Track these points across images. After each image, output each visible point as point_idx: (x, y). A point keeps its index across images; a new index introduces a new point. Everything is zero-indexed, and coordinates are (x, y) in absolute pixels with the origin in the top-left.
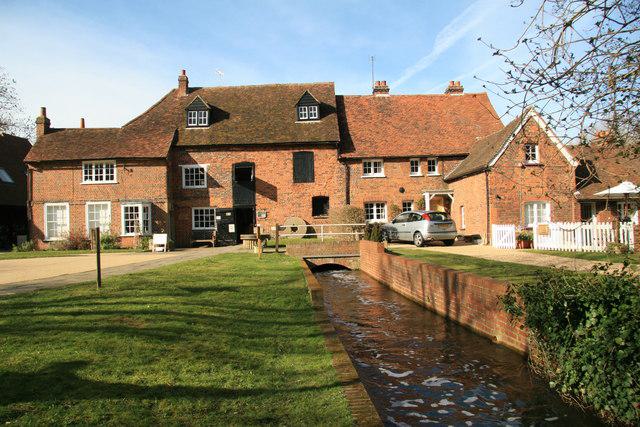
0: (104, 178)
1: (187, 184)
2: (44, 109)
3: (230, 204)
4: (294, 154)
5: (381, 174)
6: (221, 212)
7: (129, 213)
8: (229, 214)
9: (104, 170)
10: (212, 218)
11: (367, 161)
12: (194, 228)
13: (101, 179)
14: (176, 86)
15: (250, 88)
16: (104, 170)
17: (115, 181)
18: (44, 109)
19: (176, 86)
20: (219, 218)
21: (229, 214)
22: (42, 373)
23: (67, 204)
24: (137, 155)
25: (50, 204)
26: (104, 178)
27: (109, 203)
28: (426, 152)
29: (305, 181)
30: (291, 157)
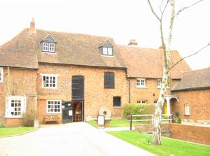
4: (105, 73)
5: (144, 86)
7: (18, 111)
8: (69, 105)
10: (59, 106)
14: (29, 27)
15: (20, 34)
19: (29, 27)
20: (64, 107)
21: (69, 105)
29: (110, 88)
30: (103, 74)
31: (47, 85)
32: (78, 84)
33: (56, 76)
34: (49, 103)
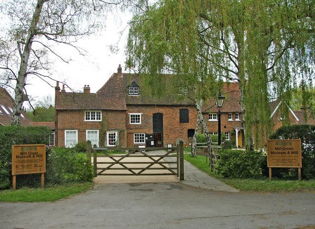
0: (90, 118)
1: (132, 122)
2: (120, 65)
3: (152, 132)
4: (180, 110)
6: (147, 136)
8: (151, 137)
9: (90, 116)
10: (143, 138)
11: (211, 114)
12: (135, 143)
13: (94, 119)
16: (90, 116)
17: (101, 120)
18: (120, 65)
21: (151, 137)
22: (24, 185)
23: (77, 131)
24: (111, 108)
25: (67, 131)
26: (90, 118)
27: (98, 131)
28: (235, 111)
31: (141, 135)
32: (158, 119)
33: (140, 114)
34: (136, 135)
